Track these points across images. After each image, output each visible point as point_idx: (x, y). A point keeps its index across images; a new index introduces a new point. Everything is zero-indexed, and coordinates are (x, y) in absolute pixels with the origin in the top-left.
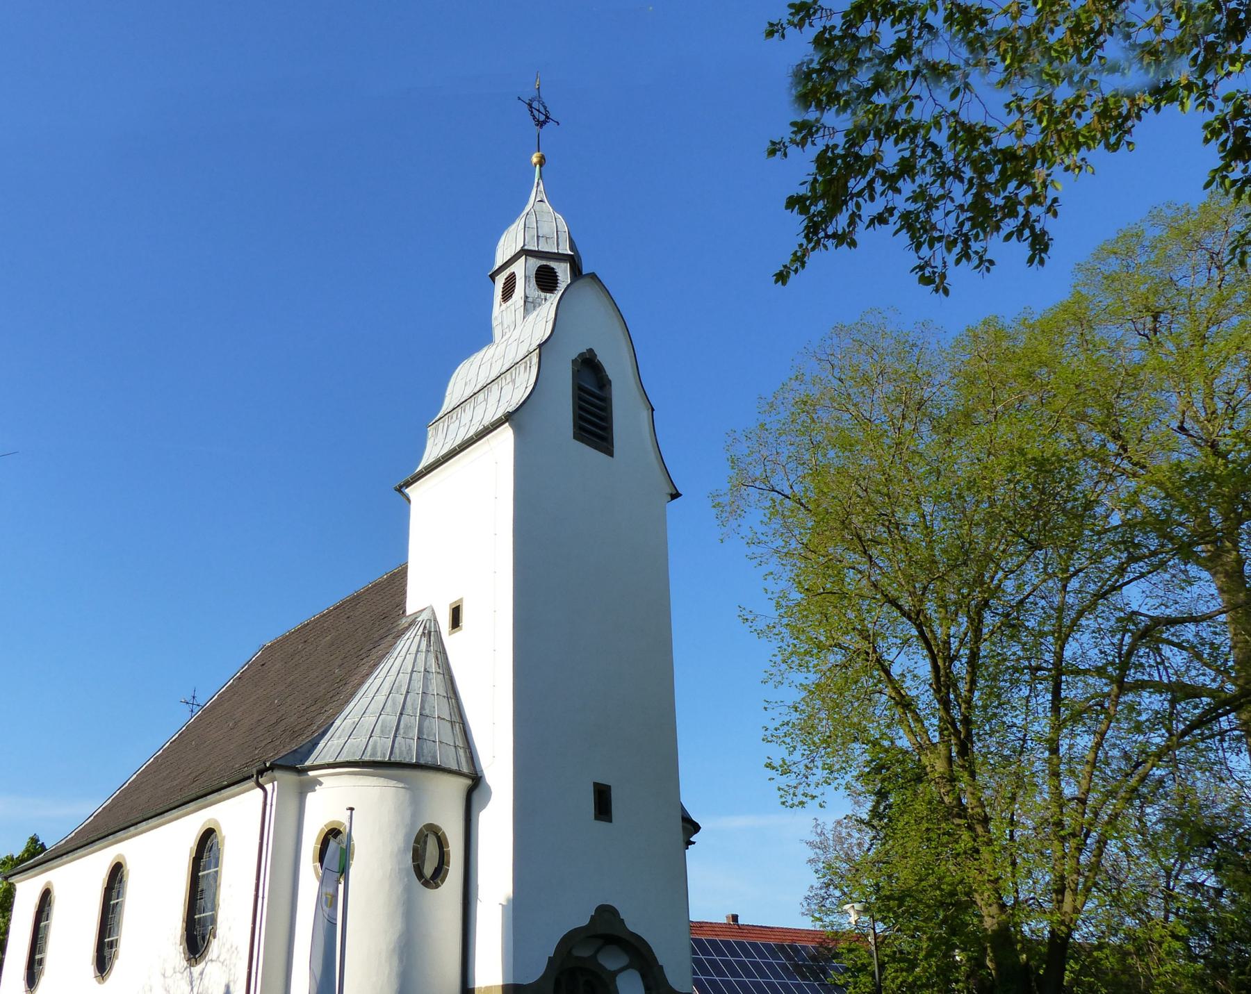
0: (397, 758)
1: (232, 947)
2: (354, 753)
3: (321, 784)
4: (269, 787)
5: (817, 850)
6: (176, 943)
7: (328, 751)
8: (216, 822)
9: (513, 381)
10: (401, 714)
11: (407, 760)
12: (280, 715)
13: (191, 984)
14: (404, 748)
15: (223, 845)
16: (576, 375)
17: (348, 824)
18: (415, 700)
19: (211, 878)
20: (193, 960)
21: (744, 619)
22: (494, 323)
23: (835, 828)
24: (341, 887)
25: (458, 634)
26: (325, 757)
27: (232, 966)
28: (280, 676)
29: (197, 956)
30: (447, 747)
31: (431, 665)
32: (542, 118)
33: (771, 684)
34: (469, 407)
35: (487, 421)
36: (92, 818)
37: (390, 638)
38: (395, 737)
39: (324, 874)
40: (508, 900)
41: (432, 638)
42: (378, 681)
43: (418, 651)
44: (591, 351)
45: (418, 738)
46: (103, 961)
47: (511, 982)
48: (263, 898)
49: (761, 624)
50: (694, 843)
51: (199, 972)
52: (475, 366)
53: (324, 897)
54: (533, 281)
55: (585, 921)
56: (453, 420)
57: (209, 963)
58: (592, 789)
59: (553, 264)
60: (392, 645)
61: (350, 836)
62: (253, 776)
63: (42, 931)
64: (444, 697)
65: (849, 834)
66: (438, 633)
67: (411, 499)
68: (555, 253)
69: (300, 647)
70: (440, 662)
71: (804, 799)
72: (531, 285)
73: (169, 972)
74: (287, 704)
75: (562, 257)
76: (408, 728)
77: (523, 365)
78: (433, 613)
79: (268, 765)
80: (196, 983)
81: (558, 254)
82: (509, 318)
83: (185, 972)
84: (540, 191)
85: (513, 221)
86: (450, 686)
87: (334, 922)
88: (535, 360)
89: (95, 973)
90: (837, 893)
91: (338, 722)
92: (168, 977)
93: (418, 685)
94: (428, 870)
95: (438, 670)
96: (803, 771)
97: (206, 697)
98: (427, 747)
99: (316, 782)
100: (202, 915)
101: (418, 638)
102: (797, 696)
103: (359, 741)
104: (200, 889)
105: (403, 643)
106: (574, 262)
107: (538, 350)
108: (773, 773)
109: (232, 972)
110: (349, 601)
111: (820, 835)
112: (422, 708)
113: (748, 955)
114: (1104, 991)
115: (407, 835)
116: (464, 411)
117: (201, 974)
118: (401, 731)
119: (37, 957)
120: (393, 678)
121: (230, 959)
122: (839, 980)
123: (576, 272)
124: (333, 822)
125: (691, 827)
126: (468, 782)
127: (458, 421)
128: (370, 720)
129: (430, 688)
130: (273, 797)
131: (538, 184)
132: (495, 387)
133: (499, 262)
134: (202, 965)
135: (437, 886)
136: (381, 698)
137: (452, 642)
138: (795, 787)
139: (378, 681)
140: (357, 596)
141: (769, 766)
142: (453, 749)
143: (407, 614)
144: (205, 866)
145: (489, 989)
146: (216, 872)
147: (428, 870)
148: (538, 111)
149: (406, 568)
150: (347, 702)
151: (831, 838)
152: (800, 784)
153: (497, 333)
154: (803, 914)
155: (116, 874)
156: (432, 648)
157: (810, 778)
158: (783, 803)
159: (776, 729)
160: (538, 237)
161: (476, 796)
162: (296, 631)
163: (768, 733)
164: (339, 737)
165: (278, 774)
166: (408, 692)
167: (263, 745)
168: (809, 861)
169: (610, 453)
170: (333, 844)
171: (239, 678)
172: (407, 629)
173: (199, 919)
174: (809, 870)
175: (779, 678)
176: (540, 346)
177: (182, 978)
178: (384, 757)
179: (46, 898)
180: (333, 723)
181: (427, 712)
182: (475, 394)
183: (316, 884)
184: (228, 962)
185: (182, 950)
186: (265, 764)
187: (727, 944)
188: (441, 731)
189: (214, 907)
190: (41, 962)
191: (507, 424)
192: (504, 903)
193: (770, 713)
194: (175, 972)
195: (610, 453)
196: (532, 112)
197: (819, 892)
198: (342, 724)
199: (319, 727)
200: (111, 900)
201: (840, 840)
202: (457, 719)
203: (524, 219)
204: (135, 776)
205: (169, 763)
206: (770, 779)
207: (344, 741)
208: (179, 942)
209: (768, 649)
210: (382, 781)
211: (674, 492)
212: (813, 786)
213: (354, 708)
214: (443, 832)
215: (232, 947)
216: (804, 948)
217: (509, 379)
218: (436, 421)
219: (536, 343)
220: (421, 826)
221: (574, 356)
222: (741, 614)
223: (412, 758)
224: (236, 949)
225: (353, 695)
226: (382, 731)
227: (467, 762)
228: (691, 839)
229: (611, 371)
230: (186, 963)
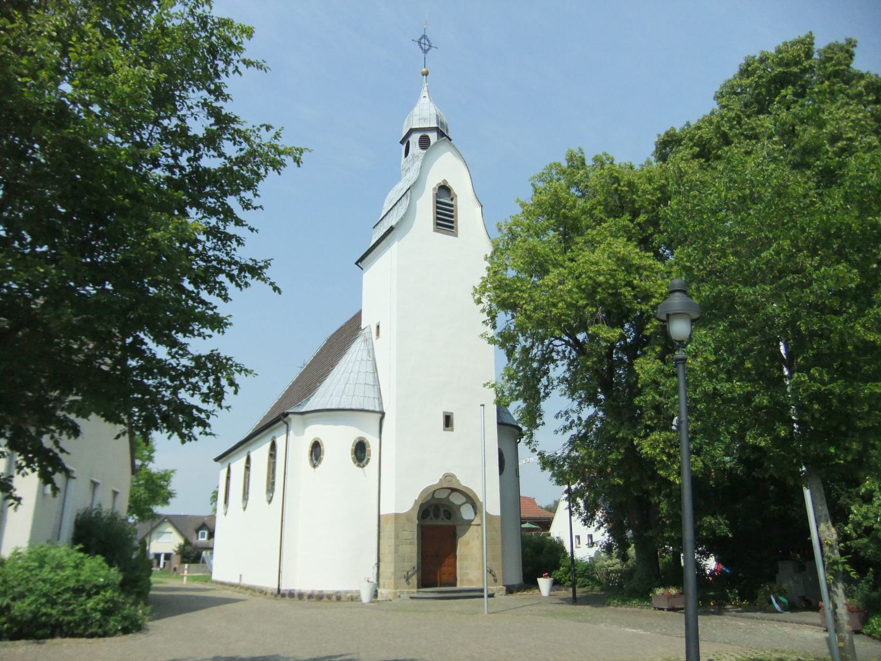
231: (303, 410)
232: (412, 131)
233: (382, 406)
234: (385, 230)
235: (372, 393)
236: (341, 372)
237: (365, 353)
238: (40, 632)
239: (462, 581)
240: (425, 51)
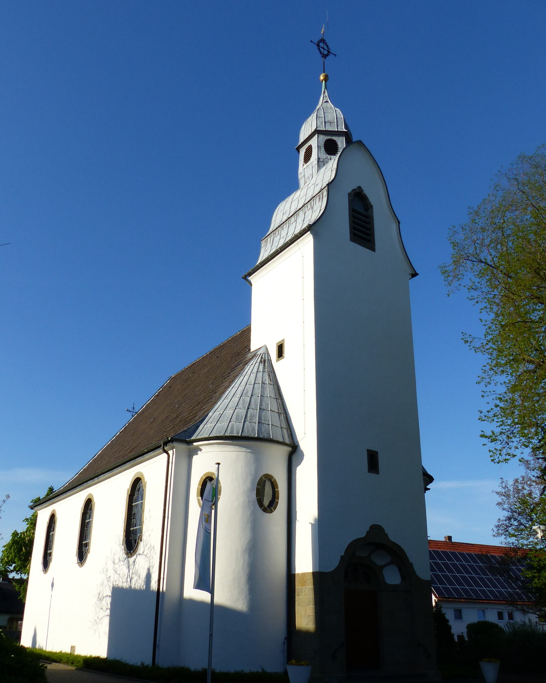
0: (245, 434)
1: (151, 546)
2: (220, 432)
3: (201, 450)
4: (170, 452)
5: (503, 497)
6: (120, 544)
7: (205, 431)
8: (141, 473)
9: (312, 208)
10: (248, 408)
11: (252, 435)
12: (178, 413)
13: (129, 568)
14: (250, 428)
15: (145, 487)
16: (351, 202)
17: (216, 473)
18: (257, 400)
19: (139, 507)
20: (130, 554)
21: (465, 341)
22: (300, 176)
23: (515, 483)
24: (213, 511)
25: (282, 361)
26: (203, 434)
27: (151, 558)
28: (179, 392)
29: (132, 552)
30: (276, 428)
31: (266, 380)
32: (326, 52)
33: (483, 384)
34: (285, 227)
35: (297, 231)
36: (78, 475)
37: (241, 365)
38: (245, 422)
39: (203, 504)
40: (315, 520)
41: (266, 364)
42: (234, 390)
43: (257, 372)
44: (359, 188)
45: (259, 422)
46: (82, 555)
47: (317, 570)
48: (168, 518)
49: (477, 344)
50: (429, 489)
51: (133, 561)
52: (288, 204)
53: (203, 516)
54: (323, 149)
55: (363, 535)
56: (276, 236)
57: (138, 556)
58: (366, 450)
59: (334, 138)
60: (243, 369)
61: (218, 478)
62: (161, 446)
63: (51, 537)
64: (274, 398)
65: (523, 488)
66: (270, 361)
67: (252, 283)
68: (336, 131)
69: (190, 376)
70: (271, 378)
71: (508, 457)
72: (322, 151)
73: (117, 561)
74: (183, 407)
75: (340, 133)
76: (252, 416)
77: (318, 197)
78: (267, 349)
79: (169, 439)
80: (131, 567)
81: (338, 131)
82: (308, 173)
83: (125, 561)
84: (326, 96)
85: (310, 116)
86: (278, 392)
87: (209, 531)
88: (325, 193)
89: (78, 561)
90: (516, 523)
91: (210, 414)
92: (116, 564)
93: (258, 392)
94: (266, 502)
95: (270, 383)
96: (506, 440)
97: (139, 407)
98: (264, 427)
99: (197, 450)
100: (134, 528)
101: (257, 364)
102: (502, 389)
103: (224, 424)
104: (133, 513)
105: (249, 367)
106: (347, 135)
107: (327, 187)
108: (486, 441)
109: (151, 561)
110: (218, 348)
111: (504, 488)
112: (261, 405)
113: (458, 560)
114: (545, 590)
115: (253, 481)
116: (283, 229)
117: (134, 562)
118: (248, 418)
119: (49, 552)
120: (243, 387)
121: (150, 554)
122: (528, 574)
123: (349, 141)
124: (208, 473)
125: (429, 479)
126: (289, 449)
127: (279, 235)
128: (229, 412)
129: (266, 393)
130: (173, 459)
131: (324, 92)
132: (301, 213)
133: (302, 140)
134: (135, 557)
135: (271, 512)
136: (236, 399)
137: (278, 366)
138: (500, 450)
139: (234, 390)
140: (223, 345)
141: (482, 436)
142: (280, 429)
143: (251, 351)
144: (136, 499)
145: (304, 574)
146: (142, 503)
147: (266, 502)
148: (323, 48)
149: (250, 327)
150: (216, 403)
151: (512, 490)
152: (504, 448)
153: (302, 182)
154: (494, 536)
155: (88, 505)
156: (266, 369)
157: (510, 444)
158: (493, 460)
159: (488, 412)
160: (325, 122)
161: (294, 458)
162: (188, 368)
163: (482, 415)
164: (211, 423)
165: (175, 444)
166: (252, 395)
167: (169, 429)
168: (498, 504)
169: (373, 249)
170: (209, 485)
171: (157, 395)
172: (251, 359)
173: (133, 530)
174: (498, 508)
175: (489, 380)
176: (328, 185)
177: (124, 565)
178: (238, 433)
179: (52, 519)
180: (208, 414)
181: (264, 407)
182: (289, 218)
183: (199, 510)
184: (148, 555)
185: (123, 548)
186: (168, 438)
187: (445, 553)
188: (272, 418)
189: (141, 524)
190: (50, 554)
191: (309, 232)
192: (313, 522)
193: (486, 399)
194: (120, 561)
195: (373, 249)
196: (319, 49)
197: (505, 522)
198: (213, 415)
199: (199, 418)
200: (86, 520)
201: (518, 491)
202: (282, 411)
203: (316, 113)
204: (101, 451)
205: (118, 443)
206: (483, 445)
207: (214, 425)
208: (121, 544)
209: (483, 359)
210: (237, 448)
211: (414, 273)
212: (513, 449)
213: (220, 405)
214: (275, 479)
215: (151, 546)
216: (494, 557)
217: (309, 207)
218: (266, 237)
219: (325, 185)
220: (262, 475)
221: (350, 191)
222: (463, 337)
223: (255, 434)
224: (153, 548)
225: (219, 398)
226: (237, 419)
227: (289, 437)
228: (428, 487)
229: (373, 199)
230: (125, 556)
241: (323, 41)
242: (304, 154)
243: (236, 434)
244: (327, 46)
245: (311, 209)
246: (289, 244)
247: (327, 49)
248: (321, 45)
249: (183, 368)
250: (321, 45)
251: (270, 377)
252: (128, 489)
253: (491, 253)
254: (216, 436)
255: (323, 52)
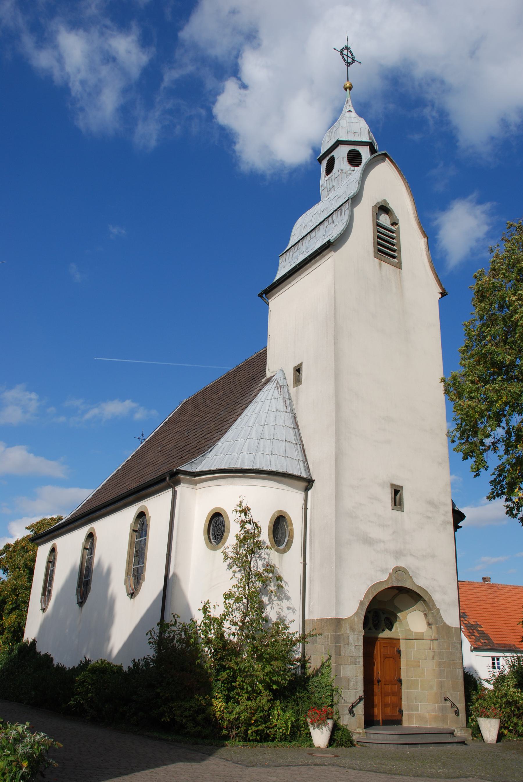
50: (461, 527)
56: (295, 251)
95: (286, 410)
123: (373, 150)
146: (145, 539)
153: (323, 193)
228: (460, 525)
231: (199, 469)
232: (338, 143)
233: (309, 472)
234: (301, 258)
235: (296, 454)
236: (251, 424)
237: (281, 402)
238: (481, 632)
239: (410, 717)
240: (349, 64)
241: (347, 48)
242: (326, 165)
243: (247, 466)
244: (352, 54)
245: (332, 223)
246: (308, 260)
247: (351, 57)
248: (345, 52)
249: (196, 392)
250: (345, 52)
251: (286, 404)
252: (131, 524)
253: (286, 442)
254: (225, 469)
255: (346, 60)
